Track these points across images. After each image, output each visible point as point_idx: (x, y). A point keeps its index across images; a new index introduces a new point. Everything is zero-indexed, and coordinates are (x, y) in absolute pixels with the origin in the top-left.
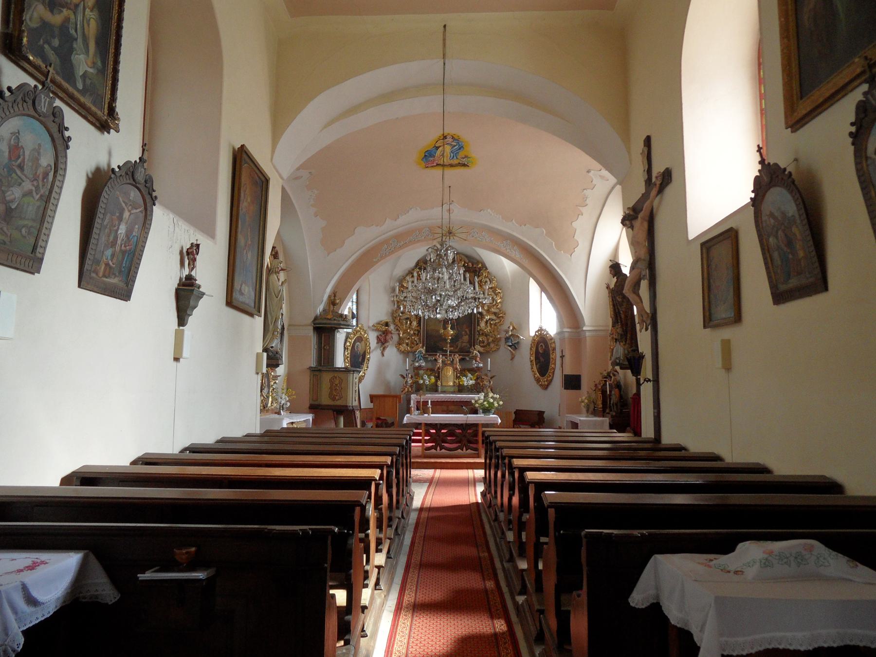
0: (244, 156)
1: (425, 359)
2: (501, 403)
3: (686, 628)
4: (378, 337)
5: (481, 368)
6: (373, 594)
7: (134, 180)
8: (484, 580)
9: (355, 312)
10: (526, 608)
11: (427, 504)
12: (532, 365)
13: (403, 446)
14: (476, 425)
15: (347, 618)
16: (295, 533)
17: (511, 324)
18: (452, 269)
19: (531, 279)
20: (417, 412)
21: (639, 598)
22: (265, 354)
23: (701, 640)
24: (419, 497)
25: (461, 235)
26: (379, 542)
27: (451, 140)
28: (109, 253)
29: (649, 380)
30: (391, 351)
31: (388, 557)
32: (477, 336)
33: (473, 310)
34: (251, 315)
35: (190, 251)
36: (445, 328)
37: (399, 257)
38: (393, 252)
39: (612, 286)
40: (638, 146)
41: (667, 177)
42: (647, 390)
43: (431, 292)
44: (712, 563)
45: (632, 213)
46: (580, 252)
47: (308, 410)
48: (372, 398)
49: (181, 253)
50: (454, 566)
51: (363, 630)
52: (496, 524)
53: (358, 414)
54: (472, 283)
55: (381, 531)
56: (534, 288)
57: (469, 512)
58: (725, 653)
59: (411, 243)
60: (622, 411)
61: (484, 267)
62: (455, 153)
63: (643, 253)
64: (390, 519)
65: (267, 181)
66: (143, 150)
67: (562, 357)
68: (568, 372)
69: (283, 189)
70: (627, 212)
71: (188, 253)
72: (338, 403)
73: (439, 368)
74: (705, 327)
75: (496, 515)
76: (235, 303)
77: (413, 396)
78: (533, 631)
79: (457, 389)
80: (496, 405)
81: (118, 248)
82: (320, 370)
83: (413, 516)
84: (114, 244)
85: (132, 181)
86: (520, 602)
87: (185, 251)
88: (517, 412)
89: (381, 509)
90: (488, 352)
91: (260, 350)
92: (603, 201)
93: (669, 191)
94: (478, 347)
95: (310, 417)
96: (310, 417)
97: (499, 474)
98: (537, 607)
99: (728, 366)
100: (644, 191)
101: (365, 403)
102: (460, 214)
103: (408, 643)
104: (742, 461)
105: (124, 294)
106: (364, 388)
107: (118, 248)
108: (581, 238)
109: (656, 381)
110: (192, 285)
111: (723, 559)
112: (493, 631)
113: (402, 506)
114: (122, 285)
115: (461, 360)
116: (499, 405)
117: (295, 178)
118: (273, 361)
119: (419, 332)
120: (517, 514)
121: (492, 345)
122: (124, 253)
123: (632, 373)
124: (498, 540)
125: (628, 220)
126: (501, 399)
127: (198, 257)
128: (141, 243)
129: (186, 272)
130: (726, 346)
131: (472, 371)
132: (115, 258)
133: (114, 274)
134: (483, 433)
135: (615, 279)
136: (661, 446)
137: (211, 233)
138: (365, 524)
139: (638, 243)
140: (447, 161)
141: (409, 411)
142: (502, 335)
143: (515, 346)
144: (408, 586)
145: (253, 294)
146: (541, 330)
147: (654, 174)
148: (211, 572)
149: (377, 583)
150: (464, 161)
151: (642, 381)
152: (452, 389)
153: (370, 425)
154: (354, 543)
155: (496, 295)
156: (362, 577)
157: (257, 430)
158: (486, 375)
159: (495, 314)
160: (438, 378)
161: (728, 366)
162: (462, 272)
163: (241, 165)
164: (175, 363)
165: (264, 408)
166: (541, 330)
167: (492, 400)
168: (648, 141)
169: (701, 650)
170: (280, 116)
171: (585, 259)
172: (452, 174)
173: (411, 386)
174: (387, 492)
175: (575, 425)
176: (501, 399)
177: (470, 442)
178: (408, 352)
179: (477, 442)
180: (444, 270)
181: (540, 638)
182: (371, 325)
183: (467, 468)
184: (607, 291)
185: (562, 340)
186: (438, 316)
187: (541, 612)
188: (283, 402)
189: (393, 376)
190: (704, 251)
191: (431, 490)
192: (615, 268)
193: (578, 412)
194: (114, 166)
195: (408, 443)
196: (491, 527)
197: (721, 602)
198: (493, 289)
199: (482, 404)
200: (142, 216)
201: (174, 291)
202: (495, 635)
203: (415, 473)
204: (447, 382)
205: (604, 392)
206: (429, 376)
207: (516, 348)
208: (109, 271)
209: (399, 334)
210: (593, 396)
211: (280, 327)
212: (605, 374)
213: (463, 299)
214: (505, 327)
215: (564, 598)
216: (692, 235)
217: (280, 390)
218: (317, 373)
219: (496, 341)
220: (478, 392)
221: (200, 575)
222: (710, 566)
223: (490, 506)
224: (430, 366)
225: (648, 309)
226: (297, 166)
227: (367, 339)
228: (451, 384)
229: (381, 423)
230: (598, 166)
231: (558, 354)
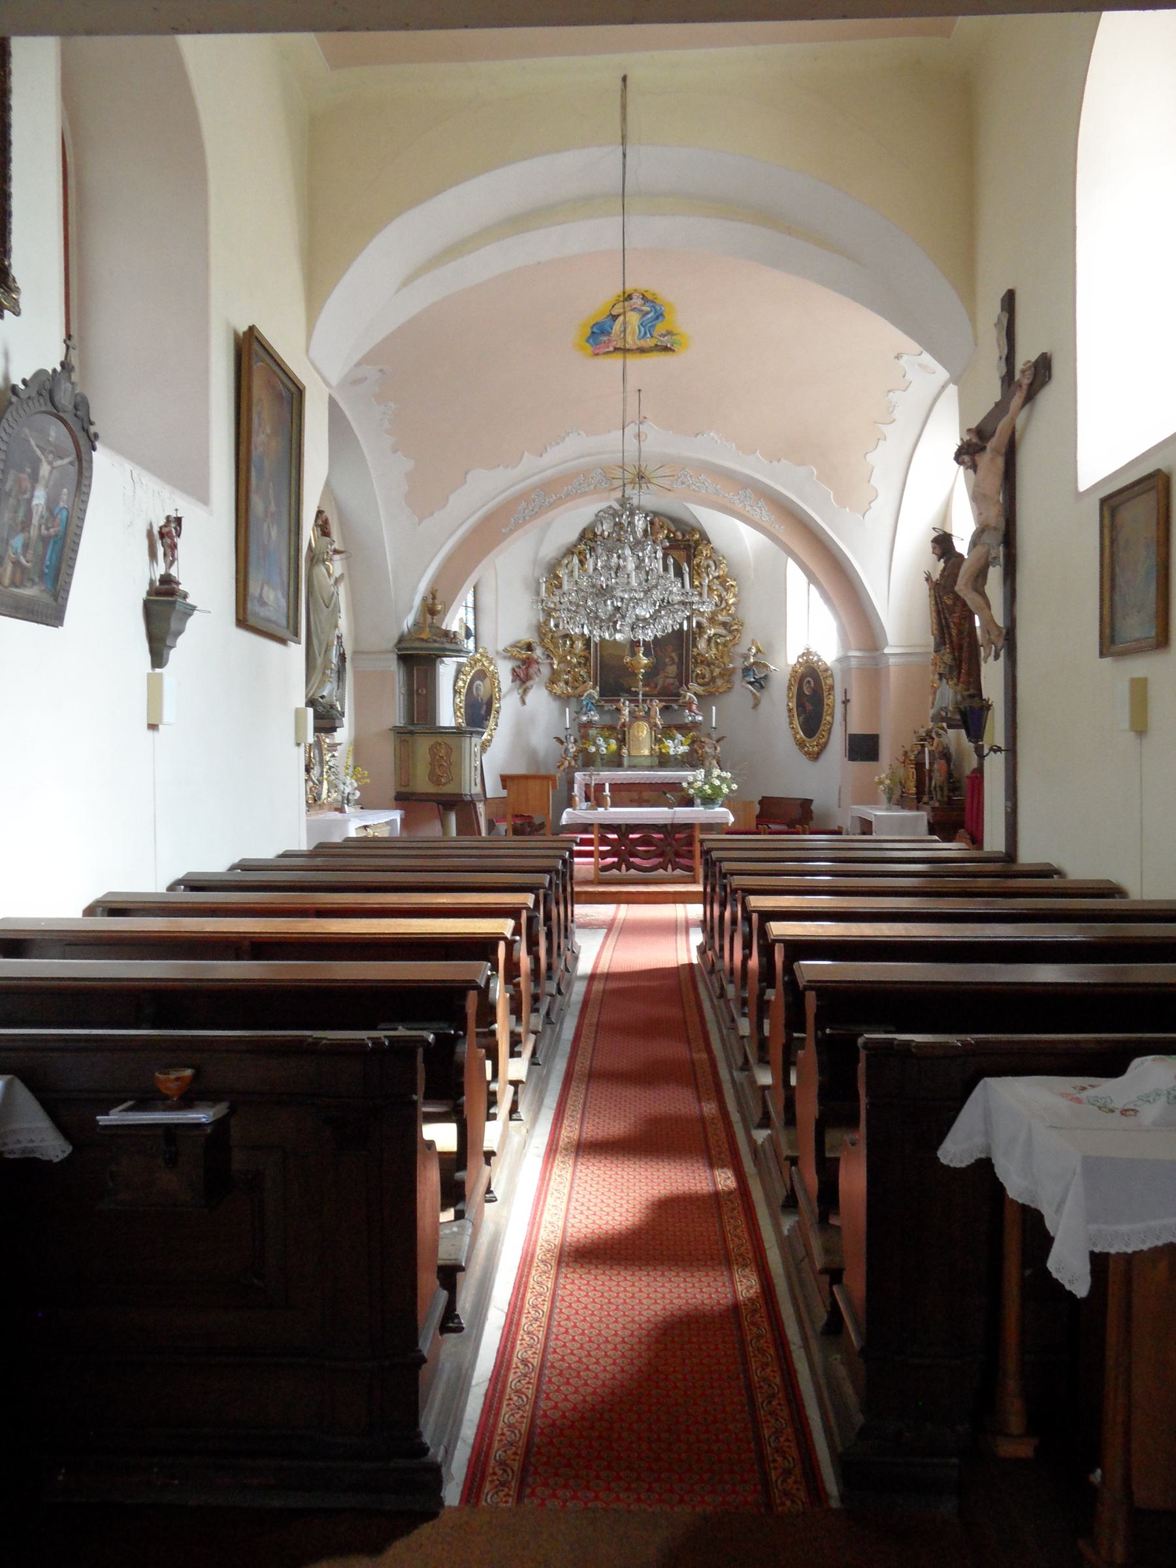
0: (256, 346)
1: (599, 709)
2: (734, 787)
3: (1033, 1206)
4: (514, 670)
5: (700, 723)
6: (505, 1128)
7: (55, 407)
8: (699, 1102)
9: (472, 627)
10: (770, 1153)
11: (603, 968)
12: (791, 717)
13: (557, 871)
14: (690, 826)
15: (459, 1175)
16: (359, 1046)
17: (753, 642)
18: (643, 550)
19: (790, 560)
20: (584, 805)
21: (956, 1150)
22: (310, 711)
23: (1057, 1228)
24: (592, 953)
25: (661, 481)
26: (515, 1041)
27: (640, 302)
28: (18, 542)
29: (999, 749)
30: (539, 696)
31: (533, 1062)
32: (691, 666)
33: (681, 625)
34: (282, 641)
35: (165, 530)
36: (634, 654)
37: (549, 524)
38: (535, 515)
39: (936, 576)
40: (992, 310)
41: (1043, 369)
42: (995, 768)
43: (604, 593)
44: (1083, 1095)
45: (975, 440)
46: (881, 509)
47: (394, 802)
48: (505, 780)
49: (150, 534)
50: (646, 1076)
51: (489, 1191)
52: (722, 1001)
53: (481, 807)
54: (679, 574)
55: (519, 1019)
56: (795, 576)
57: (672, 984)
58: (1097, 1250)
59: (570, 497)
60: (952, 805)
61: (705, 539)
62: (647, 329)
63: (995, 515)
64: (536, 998)
65: (301, 392)
66: (68, 347)
67: (846, 702)
68: (856, 728)
69: (333, 404)
70: (967, 438)
71: (162, 535)
72: (449, 789)
73: (624, 725)
74: (1102, 654)
75: (722, 988)
76: (252, 621)
77: (578, 776)
78: (781, 1193)
79: (656, 761)
80: (725, 790)
81: (34, 532)
82: (412, 733)
83: (579, 989)
84: (26, 525)
85: (50, 408)
86: (760, 1141)
87: (156, 530)
88: (765, 802)
89: (518, 985)
90: (711, 694)
91: (301, 702)
92: (924, 413)
93: (1048, 397)
94: (693, 686)
95: (396, 815)
96: (396, 815)
97: (727, 914)
98: (786, 1152)
99: (1140, 728)
100: (998, 398)
101: (493, 789)
102: (659, 442)
103: (568, 1210)
104: (1163, 898)
105: (50, 612)
106: (491, 761)
107: (34, 532)
108: (884, 485)
109: (1011, 751)
110: (172, 593)
111: (1106, 1087)
112: (711, 1189)
113: (557, 976)
114: (47, 598)
115: (665, 710)
116: (731, 790)
117: (353, 381)
118: (326, 721)
119: (587, 659)
120: (756, 990)
121: (719, 682)
122: (45, 540)
123: (968, 735)
124: (725, 1031)
125: (968, 454)
126: (734, 780)
127: (180, 542)
128: (75, 521)
129: (160, 569)
130: (1139, 690)
131: (683, 728)
132: (31, 552)
133: (32, 581)
134: (702, 841)
135: (942, 564)
136: (1016, 868)
137: (202, 496)
138: (488, 1013)
139: (985, 496)
140: (631, 341)
141: (570, 803)
142: (738, 664)
143: (760, 684)
144: (568, 1112)
145: (283, 603)
146: (808, 653)
147: (1019, 365)
148: (221, 1109)
149: (514, 1109)
150: (666, 341)
151: (986, 751)
152: (648, 762)
153: (502, 827)
154: (468, 1049)
155: (727, 590)
156: (484, 1105)
157: (302, 844)
158: (709, 736)
159: (724, 625)
160: (622, 742)
161: (1140, 728)
162: (660, 554)
163: (250, 367)
164: (150, 733)
165: (314, 802)
166: (808, 653)
167: (717, 782)
168: (1009, 301)
169: (1056, 1245)
170: (321, 263)
171: (890, 522)
172: (643, 367)
173: (575, 757)
174: (529, 952)
175: (866, 827)
176: (734, 780)
177: (678, 855)
178: (569, 697)
179: (690, 855)
180: (628, 552)
181: (791, 1203)
182: (501, 648)
183: (675, 902)
184: (925, 586)
185: (846, 672)
186: (618, 636)
187: (794, 1161)
188: (347, 790)
189: (541, 739)
190: (1107, 514)
191: (611, 941)
192: (943, 543)
193: (873, 801)
194: (16, 380)
195: (568, 864)
196: (713, 1007)
197: (1093, 1168)
198: (722, 580)
199: (701, 790)
200: (73, 470)
201: (141, 602)
202: (716, 1195)
203: (581, 911)
204: (640, 749)
205: (919, 765)
206: (606, 739)
207: (762, 687)
208: (22, 576)
209: (551, 665)
210: (901, 772)
211: (335, 660)
212: (922, 732)
213: (666, 604)
214: (742, 649)
215: (831, 1136)
216: (1084, 484)
217: (341, 770)
218: (407, 737)
219: (727, 674)
220: (694, 766)
221: (201, 1116)
222: (1079, 1101)
223: (712, 971)
224: (608, 720)
225: (1000, 620)
226: (357, 357)
227: (494, 675)
228: (646, 752)
229: (525, 826)
230: (915, 347)
231: (838, 696)
